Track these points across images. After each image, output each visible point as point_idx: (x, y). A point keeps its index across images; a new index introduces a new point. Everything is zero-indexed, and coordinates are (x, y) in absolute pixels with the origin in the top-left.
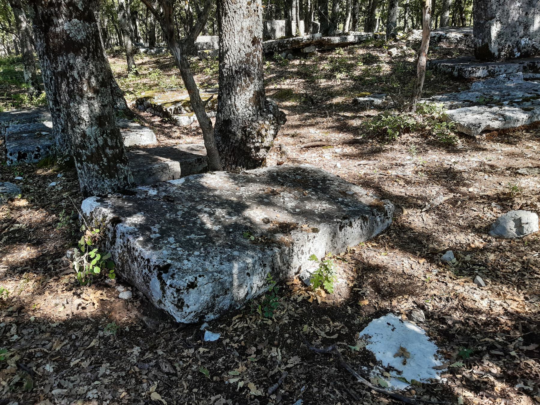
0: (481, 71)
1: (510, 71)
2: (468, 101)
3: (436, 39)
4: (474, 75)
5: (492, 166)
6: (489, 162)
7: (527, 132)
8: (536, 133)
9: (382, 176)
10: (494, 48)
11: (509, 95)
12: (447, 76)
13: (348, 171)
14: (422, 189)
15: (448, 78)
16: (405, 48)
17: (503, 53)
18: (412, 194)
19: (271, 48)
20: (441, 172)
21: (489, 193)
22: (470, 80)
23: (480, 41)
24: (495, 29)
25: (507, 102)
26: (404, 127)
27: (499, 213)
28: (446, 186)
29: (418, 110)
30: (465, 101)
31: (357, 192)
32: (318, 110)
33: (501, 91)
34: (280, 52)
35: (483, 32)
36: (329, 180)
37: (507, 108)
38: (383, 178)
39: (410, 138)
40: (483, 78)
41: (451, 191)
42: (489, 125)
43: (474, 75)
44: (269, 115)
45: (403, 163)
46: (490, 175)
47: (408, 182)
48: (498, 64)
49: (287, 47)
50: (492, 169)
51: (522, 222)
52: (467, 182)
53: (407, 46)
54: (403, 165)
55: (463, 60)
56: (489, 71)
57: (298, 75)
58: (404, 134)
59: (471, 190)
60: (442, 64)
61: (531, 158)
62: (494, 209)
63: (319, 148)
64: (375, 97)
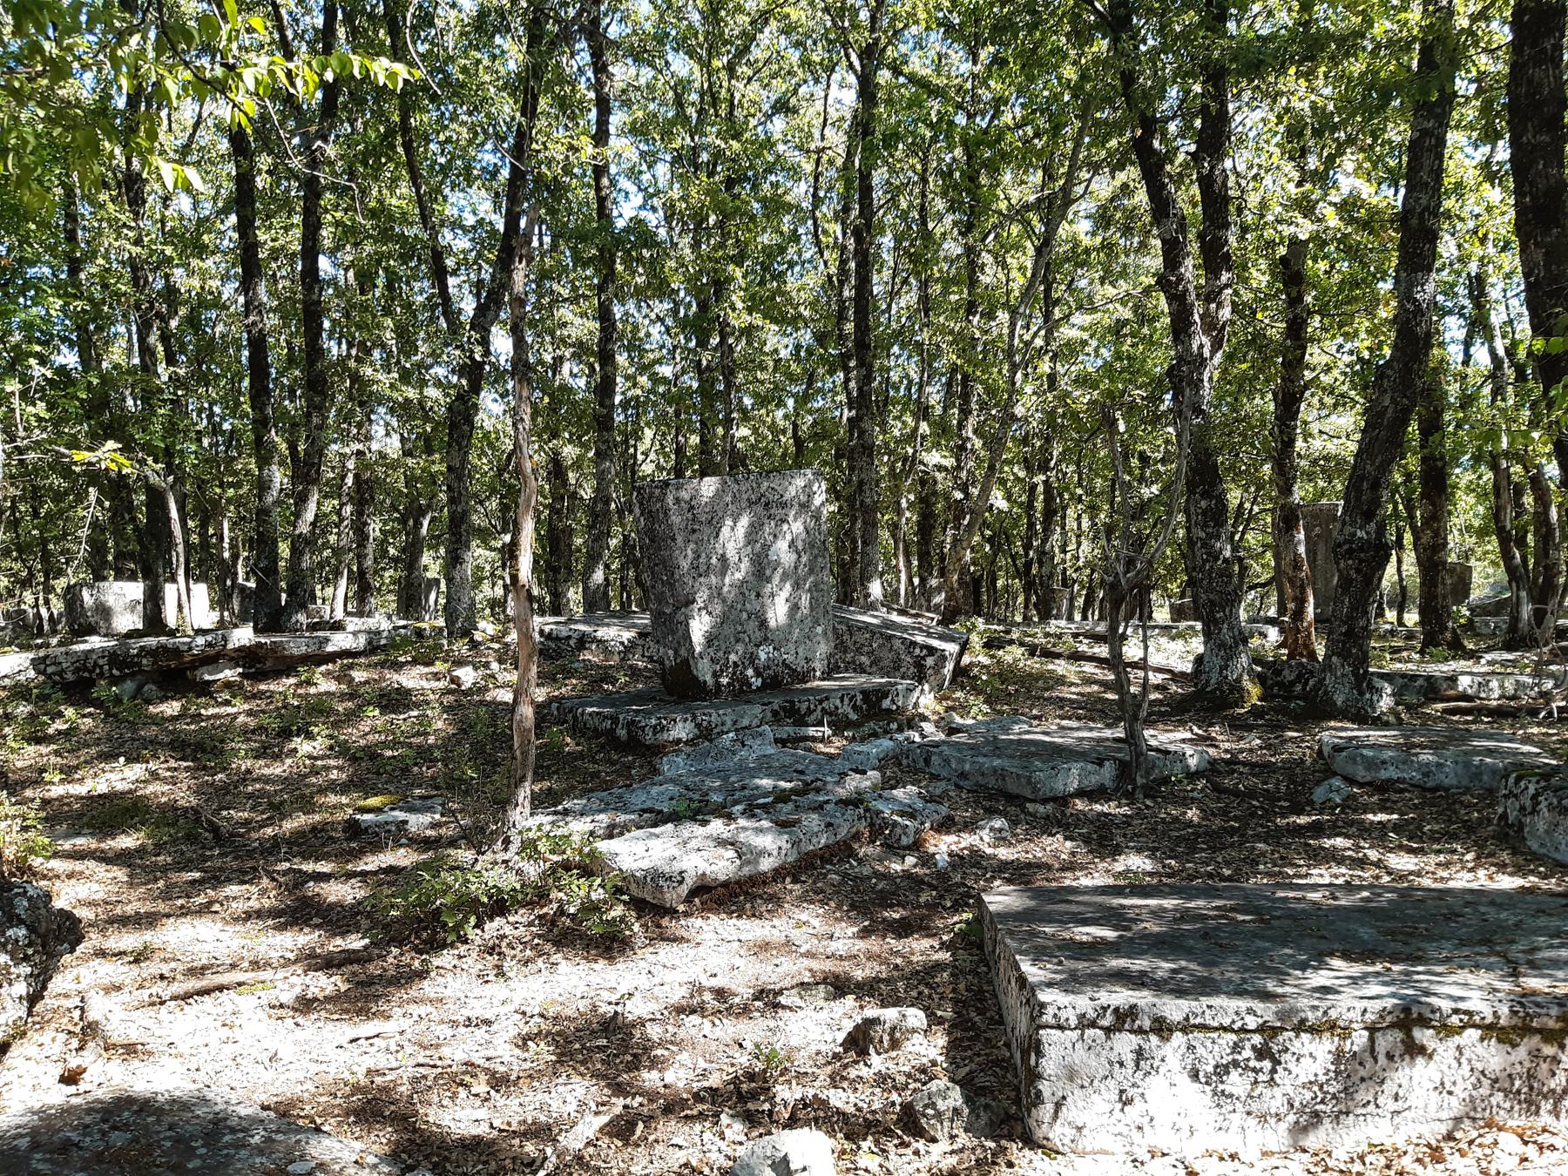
0: (680, 725)
1: (745, 722)
2: (650, 810)
3: (572, 642)
4: (665, 736)
5: (720, 994)
6: (714, 983)
7: (794, 882)
8: (815, 882)
9: (421, 1070)
10: (704, 671)
11: (744, 788)
12: (602, 740)
13: (314, 1068)
14: (540, 1096)
15: (602, 751)
16: (495, 666)
17: (725, 681)
18: (509, 1124)
19: (85, 669)
20: (593, 1032)
21: (715, 1081)
22: (659, 750)
23: (671, 652)
24: (699, 627)
25: (739, 808)
26: (490, 898)
27: (741, 1143)
28: (604, 1077)
29: (523, 848)
30: (644, 811)
31: (327, 1158)
32: (235, 858)
33: (725, 779)
34: (114, 681)
35: (673, 633)
36: (233, 1130)
37: (742, 822)
38: (425, 1077)
39: (508, 930)
40: (686, 743)
41: (619, 1089)
42: (704, 874)
43: (665, 736)
44: (10, 933)
45: (489, 1015)
46: (717, 1022)
47: (499, 1082)
48: (717, 708)
49: (139, 664)
50: (723, 1003)
51: (793, 1167)
52: (659, 1052)
53: (500, 661)
54: (488, 1023)
55: (638, 698)
56: (698, 726)
57: (173, 749)
58: (492, 920)
59: (670, 1077)
60: (590, 710)
61: (810, 955)
62: (728, 1133)
63: (224, 996)
64: (412, 810)
